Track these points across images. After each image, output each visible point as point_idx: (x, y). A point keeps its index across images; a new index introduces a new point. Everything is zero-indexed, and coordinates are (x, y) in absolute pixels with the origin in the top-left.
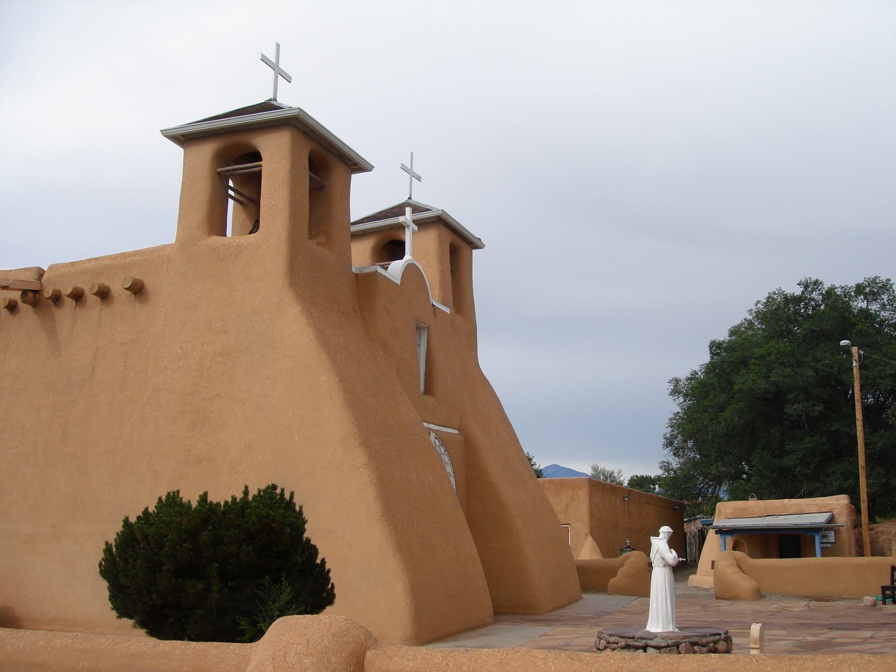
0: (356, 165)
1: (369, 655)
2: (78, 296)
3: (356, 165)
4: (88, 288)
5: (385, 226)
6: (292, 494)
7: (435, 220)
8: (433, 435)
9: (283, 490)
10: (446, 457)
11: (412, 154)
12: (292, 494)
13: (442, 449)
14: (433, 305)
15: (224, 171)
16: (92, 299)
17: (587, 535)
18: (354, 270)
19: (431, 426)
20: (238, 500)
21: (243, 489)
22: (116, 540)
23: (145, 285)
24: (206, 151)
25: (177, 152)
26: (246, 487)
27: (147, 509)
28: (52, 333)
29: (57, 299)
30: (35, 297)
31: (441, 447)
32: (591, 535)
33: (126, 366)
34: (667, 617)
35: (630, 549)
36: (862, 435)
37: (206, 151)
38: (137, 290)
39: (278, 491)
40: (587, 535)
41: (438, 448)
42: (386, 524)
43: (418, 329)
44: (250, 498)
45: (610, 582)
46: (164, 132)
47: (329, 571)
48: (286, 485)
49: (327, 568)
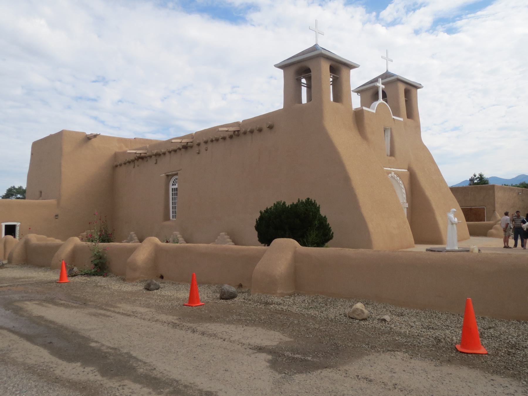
0: (349, 66)
3: (349, 66)
4: (265, 127)
6: (315, 201)
7: (396, 80)
8: (393, 173)
9: (311, 200)
10: (400, 181)
12: (315, 201)
13: (398, 178)
14: (393, 118)
18: (353, 109)
19: (392, 169)
20: (276, 204)
21: (298, 200)
22: (259, 218)
25: (281, 72)
26: (299, 199)
27: (267, 208)
30: (238, 133)
31: (398, 178)
37: (292, 70)
39: (310, 200)
41: (396, 178)
43: (385, 130)
45: (153, 238)
47: (330, 228)
48: (313, 198)
49: (329, 227)
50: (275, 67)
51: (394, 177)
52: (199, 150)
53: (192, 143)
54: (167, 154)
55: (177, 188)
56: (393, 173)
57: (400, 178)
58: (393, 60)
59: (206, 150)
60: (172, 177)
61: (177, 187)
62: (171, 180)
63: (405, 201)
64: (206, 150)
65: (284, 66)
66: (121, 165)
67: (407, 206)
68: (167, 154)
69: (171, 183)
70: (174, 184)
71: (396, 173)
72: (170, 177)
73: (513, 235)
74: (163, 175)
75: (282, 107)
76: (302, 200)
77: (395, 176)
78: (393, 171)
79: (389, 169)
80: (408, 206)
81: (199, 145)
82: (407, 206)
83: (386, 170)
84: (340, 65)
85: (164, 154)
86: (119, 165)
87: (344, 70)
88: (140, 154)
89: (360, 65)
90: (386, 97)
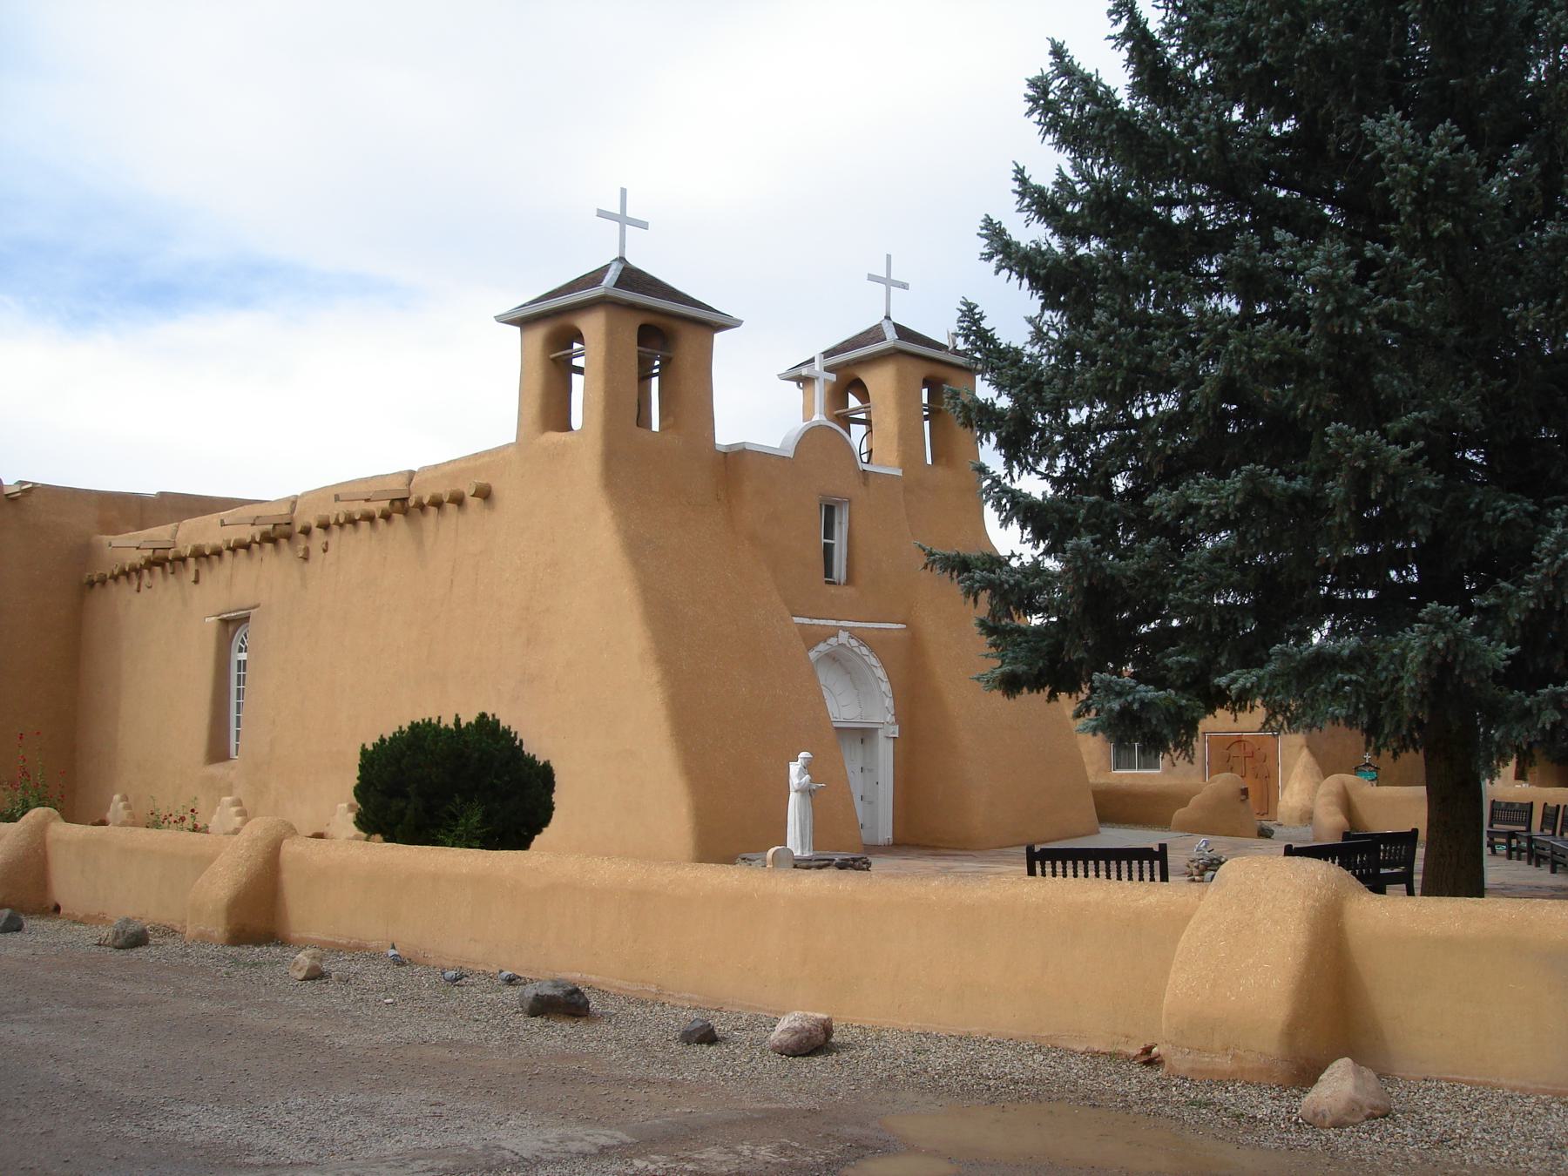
1: (285, 842)
2: (438, 503)
4: (468, 490)
5: (841, 363)
11: (889, 257)
12: (493, 715)
15: (560, 356)
16: (473, 503)
17: (1302, 747)
19: (842, 623)
23: (493, 489)
24: (539, 333)
28: (420, 544)
29: (421, 507)
30: (403, 505)
31: (861, 648)
32: (1308, 747)
33: (476, 579)
34: (795, 842)
35: (1372, 769)
36: (231, 712)
37: (539, 333)
38: (485, 494)
40: (1302, 747)
42: (674, 744)
44: (1048, 689)
46: (498, 318)
50: (497, 321)
51: (848, 645)
52: (307, 550)
53: (287, 526)
54: (227, 554)
55: (245, 661)
56: (843, 637)
57: (872, 650)
58: (908, 284)
59: (325, 551)
60: (240, 626)
61: (245, 659)
62: (235, 633)
63: (890, 718)
64: (325, 551)
65: (525, 321)
66: (115, 578)
67: (894, 733)
68: (227, 554)
69: (236, 643)
70: (243, 646)
71: (852, 633)
72: (231, 629)
73: (1503, 844)
74: (213, 618)
75: (514, 440)
76: (1070, 697)
77: (854, 643)
78: (844, 629)
79: (833, 623)
80: (897, 732)
81: (307, 531)
82: (894, 733)
83: (819, 625)
84: (676, 325)
85: (218, 553)
86: (191, 556)
87: (688, 340)
88: (152, 551)
89: (742, 321)
90: (869, 402)
